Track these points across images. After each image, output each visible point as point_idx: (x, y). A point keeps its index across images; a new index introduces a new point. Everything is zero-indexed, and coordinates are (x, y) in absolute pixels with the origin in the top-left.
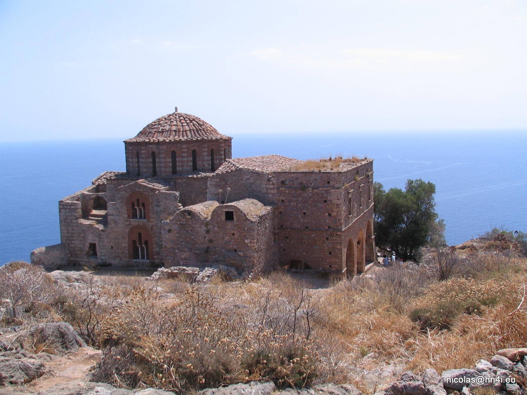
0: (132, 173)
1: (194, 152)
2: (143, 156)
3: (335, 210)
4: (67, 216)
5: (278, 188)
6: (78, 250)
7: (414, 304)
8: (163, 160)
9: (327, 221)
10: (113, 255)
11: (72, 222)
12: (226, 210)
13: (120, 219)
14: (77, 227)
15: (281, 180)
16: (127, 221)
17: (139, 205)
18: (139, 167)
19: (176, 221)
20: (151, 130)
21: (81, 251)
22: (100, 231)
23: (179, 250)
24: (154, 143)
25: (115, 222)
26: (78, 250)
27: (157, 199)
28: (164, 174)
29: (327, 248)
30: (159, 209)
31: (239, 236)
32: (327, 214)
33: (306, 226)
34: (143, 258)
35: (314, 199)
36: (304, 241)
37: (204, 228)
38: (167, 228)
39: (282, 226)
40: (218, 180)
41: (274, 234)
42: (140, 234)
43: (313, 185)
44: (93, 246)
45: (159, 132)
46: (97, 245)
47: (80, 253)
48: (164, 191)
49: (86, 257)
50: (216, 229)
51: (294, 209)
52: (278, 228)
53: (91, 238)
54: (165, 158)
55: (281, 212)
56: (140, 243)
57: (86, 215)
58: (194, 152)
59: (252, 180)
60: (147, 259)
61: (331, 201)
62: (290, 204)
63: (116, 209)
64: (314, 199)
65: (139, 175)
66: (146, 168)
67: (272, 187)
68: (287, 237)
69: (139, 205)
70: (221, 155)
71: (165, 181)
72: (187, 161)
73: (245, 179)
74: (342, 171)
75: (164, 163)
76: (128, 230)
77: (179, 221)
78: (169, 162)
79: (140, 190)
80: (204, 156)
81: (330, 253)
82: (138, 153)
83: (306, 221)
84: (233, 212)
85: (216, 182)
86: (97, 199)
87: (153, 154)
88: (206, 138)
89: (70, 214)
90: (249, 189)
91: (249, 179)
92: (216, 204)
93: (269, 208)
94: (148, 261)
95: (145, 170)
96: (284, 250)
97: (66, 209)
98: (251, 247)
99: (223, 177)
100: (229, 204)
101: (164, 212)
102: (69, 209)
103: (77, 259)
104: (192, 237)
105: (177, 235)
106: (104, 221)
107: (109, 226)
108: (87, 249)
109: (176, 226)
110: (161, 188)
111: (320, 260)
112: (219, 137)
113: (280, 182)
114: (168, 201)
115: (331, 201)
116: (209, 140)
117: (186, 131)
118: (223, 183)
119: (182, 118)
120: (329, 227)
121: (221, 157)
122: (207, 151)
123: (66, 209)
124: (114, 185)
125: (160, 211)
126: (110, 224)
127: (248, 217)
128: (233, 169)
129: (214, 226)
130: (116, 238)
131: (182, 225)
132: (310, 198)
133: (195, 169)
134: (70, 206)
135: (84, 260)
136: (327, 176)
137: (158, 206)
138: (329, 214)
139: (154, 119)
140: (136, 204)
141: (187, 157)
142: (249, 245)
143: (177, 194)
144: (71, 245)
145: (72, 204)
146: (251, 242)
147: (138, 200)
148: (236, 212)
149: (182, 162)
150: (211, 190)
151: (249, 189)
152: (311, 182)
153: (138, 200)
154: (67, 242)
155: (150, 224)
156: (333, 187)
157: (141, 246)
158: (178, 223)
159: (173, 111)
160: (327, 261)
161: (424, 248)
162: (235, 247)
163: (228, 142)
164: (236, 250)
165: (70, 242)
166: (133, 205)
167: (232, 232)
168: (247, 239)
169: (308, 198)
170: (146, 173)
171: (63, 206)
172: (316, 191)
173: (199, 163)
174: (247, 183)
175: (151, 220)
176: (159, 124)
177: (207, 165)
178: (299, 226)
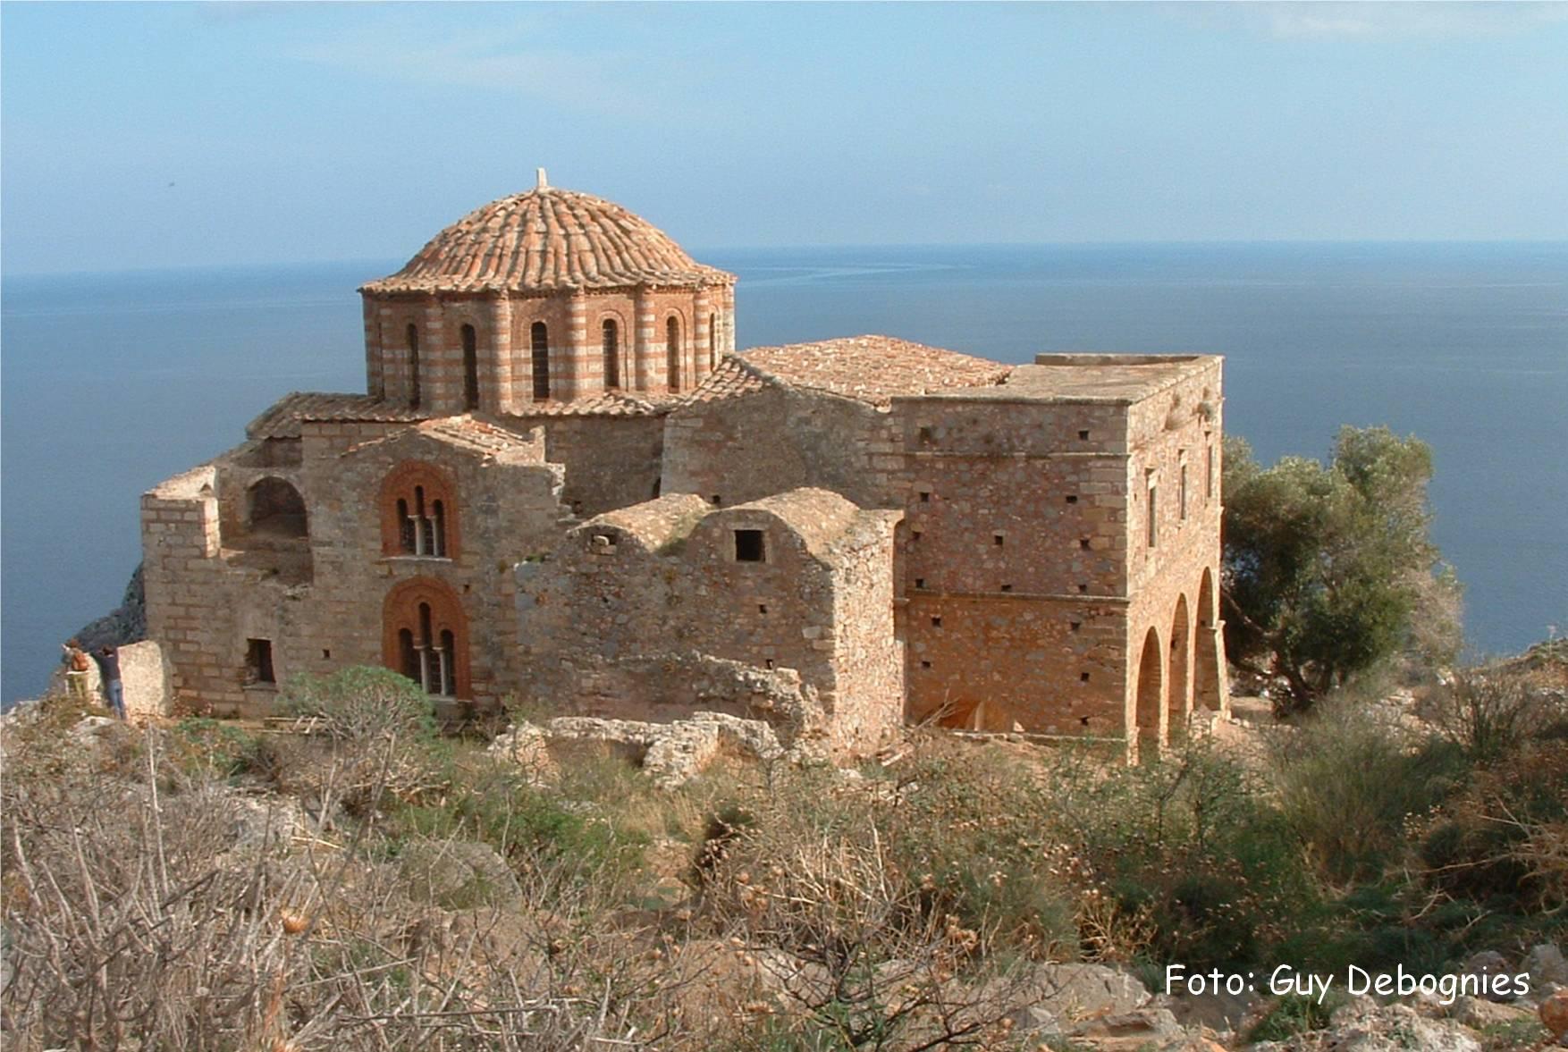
3: (1103, 528)
4: (169, 546)
6: (209, 665)
9: (1077, 567)
11: (186, 569)
12: (741, 527)
13: (354, 558)
15: (921, 424)
16: (380, 563)
19: (566, 563)
21: (219, 666)
23: (574, 661)
24: (468, 295)
25: (338, 566)
26: (209, 665)
27: (487, 490)
29: (1073, 659)
30: (491, 523)
31: (784, 616)
32: (1076, 544)
33: (1003, 582)
35: (1034, 491)
36: (994, 634)
37: (660, 589)
39: (920, 583)
43: (1029, 442)
46: (273, 644)
47: (215, 672)
49: (236, 687)
51: (964, 525)
55: (917, 535)
56: (427, 638)
59: (818, 425)
60: (451, 692)
61: (1090, 497)
62: (949, 507)
64: (1034, 491)
67: (887, 448)
68: (936, 622)
76: (384, 594)
77: (576, 563)
81: (1085, 677)
82: (412, 330)
83: (1002, 565)
84: (759, 532)
85: (696, 431)
87: (468, 330)
89: (180, 540)
90: (809, 454)
91: (807, 421)
92: (703, 506)
94: (451, 700)
96: (926, 664)
97: (167, 522)
100: (749, 506)
101: (510, 532)
102: (176, 522)
103: (204, 695)
104: (622, 618)
105: (568, 610)
107: (316, 581)
108: (240, 660)
109: (564, 581)
111: (1051, 698)
113: (917, 432)
114: (525, 495)
115: (1090, 497)
118: (719, 435)
123: (167, 522)
124: (331, 438)
125: (497, 531)
129: (697, 581)
130: (344, 623)
131: (587, 576)
132: (1020, 487)
134: (183, 511)
135: (228, 697)
136: (1079, 413)
137: (490, 511)
138: (1085, 544)
140: (412, 504)
142: (816, 645)
144: (182, 647)
147: (419, 490)
151: (809, 454)
152: (1023, 432)
153: (419, 490)
154: (171, 636)
155: (460, 573)
157: (429, 649)
158: (572, 569)
160: (1074, 703)
165: (180, 636)
166: (402, 505)
167: (760, 601)
168: (811, 624)
169: (1013, 486)
172: (1039, 463)
175: (465, 559)
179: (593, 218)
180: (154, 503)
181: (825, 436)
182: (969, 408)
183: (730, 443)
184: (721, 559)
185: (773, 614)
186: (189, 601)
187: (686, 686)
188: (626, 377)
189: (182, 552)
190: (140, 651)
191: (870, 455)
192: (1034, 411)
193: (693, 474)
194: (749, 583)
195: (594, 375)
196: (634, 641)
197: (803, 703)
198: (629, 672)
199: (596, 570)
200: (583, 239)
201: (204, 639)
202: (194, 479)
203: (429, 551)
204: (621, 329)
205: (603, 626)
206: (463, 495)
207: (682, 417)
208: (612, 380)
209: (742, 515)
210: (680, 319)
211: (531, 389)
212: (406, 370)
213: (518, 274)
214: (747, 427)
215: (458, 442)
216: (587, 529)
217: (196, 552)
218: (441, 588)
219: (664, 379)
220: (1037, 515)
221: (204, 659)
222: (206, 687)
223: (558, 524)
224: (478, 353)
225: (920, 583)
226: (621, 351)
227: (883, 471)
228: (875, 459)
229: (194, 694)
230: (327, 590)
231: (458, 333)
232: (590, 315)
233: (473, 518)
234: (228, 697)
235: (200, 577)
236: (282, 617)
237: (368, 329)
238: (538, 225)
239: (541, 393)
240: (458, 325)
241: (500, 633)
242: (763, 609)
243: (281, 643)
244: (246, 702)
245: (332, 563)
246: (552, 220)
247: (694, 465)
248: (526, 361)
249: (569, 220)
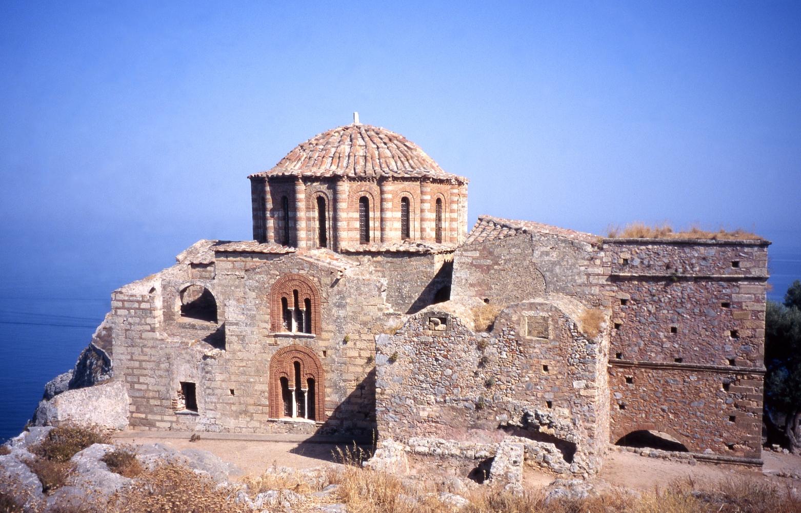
4: (130, 324)
6: (153, 398)
7: (33, 456)
10: (234, 408)
11: (141, 338)
13: (252, 332)
16: (268, 336)
21: (162, 399)
23: (415, 399)
25: (242, 338)
26: (153, 398)
33: (677, 356)
34: (301, 414)
40: (477, 254)
46: (197, 385)
47: (158, 402)
58: (405, 200)
61: (739, 304)
76: (271, 356)
77: (417, 335)
79: (302, 272)
89: (137, 320)
91: (547, 254)
97: (128, 309)
101: (354, 319)
102: (135, 309)
103: (150, 417)
115: (739, 304)
118: (489, 262)
123: (128, 309)
126: (231, 343)
130: (244, 373)
131: (425, 344)
134: (139, 302)
137: (340, 306)
138: (734, 334)
142: (582, 392)
144: (136, 386)
146: (587, 387)
151: (548, 274)
153: (296, 292)
154: (129, 379)
155: (322, 344)
158: (415, 339)
165: (136, 380)
166: (284, 301)
167: (544, 362)
168: (578, 379)
179: (390, 140)
180: (121, 297)
181: (559, 263)
183: (496, 267)
184: (518, 334)
185: (553, 370)
186: (142, 358)
187: (492, 417)
188: (414, 233)
189: (141, 328)
190: (108, 389)
191: (588, 275)
192: (702, 249)
193: (472, 285)
194: (537, 350)
195: (396, 229)
196: (456, 387)
197: (575, 432)
198: (453, 408)
199: (431, 340)
200: (387, 151)
201: (150, 382)
202: (146, 283)
203: (300, 329)
204: (412, 204)
205: (435, 377)
206: (324, 295)
207: (466, 250)
208: (406, 232)
210: (443, 200)
211: (358, 236)
213: (351, 166)
214: (508, 257)
215: (320, 263)
216: (426, 314)
217: (148, 328)
219: (433, 234)
221: (151, 394)
222: (152, 412)
223: (384, 314)
226: (411, 215)
227: (596, 285)
228: (591, 278)
229: (143, 416)
230: (234, 352)
232: (395, 194)
233: (330, 310)
234: (166, 418)
235: (150, 343)
236: (203, 369)
237: (254, 200)
238: (360, 142)
239: (365, 238)
241: (344, 381)
242: (546, 368)
243: (202, 385)
244: (177, 422)
245: (237, 336)
246: (367, 139)
247: (472, 280)
248: (356, 219)
249: (377, 140)
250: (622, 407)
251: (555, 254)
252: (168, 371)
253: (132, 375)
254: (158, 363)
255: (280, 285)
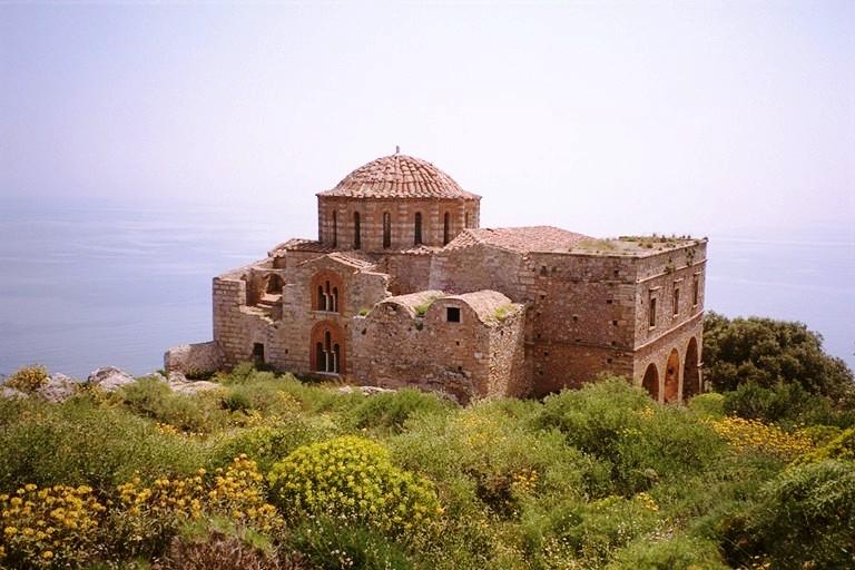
0: (327, 243)
1: (418, 214)
2: (341, 217)
5: (536, 278)
8: (372, 226)
12: (450, 306)
14: (238, 318)
17: (328, 291)
18: (335, 234)
20: (356, 180)
22: (269, 326)
24: (357, 199)
28: (371, 247)
30: (357, 298)
32: (611, 322)
38: (361, 328)
39: (539, 336)
40: (446, 259)
41: (526, 347)
42: (328, 334)
44: (259, 348)
45: (368, 182)
48: (367, 272)
50: (432, 333)
52: (534, 340)
53: (257, 336)
54: (373, 222)
56: (328, 348)
57: (253, 300)
58: (418, 214)
61: (618, 301)
63: (296, 295)
65: (334, 246)
66: (346, 235)
68: (546, 354)
69: (328, 291)
70: (461, 222)
71: (372, 256)
72: (407, 229)
73: (486, 260)
74: (640, 256)
75: (373, 233)
77: (379, 318)
78: (380, 229)
80: (432, 222)
82: (335, 213)
86: (266, 282)
87: (357, 214)
88: (437, 195)
91: (492, 261)
93: (519, 307)
95: (344, 239)
96: (541, 373)
98: (483, 365)
99: (454, 257)
101: (365, 303)
104: (397, 344)
106: (277, 310)
107: (284, 319)
110: (366, 267)
112: (458, 194)
115: (618, 301)
116: (442, 199)
117: (408, 183)
119: (404, 163)
120: (614, 343)
121: (459, 225)
122: (439, 215)
125: (359, 302)
127: (481, 318)
128: (471, 244)
133: (418, 241)
137: (356, 294)
138: (615, 323)
139: (364, 163)
140: (324, 289)
141: (407, 222)
142: (480, 361)
143: (386, 277)
145: (232, 284)
146: (483, 358)
147: (328, 282)
148: (464, 312)
149: (399, 229)
150: (436, 274)
156: (624, 281)
159: (392, 152)
161: (327, 416)
162: (460, 363)
163: (474, 202)
164: (460, 368)
166: (320, 288)
167: (457, 340)
168: (478, 352)
170: (344, 243)
171: (219, 286)
172: (595, 285)
173: (425, 234)
174: (486, 267)
176: (369, 171)
177: (438, 235)
178: (566, 338)
179: (418, 169)
182: (564, 258)
184: (440, 320)
185: (462, 346)
203: (331, 309)
209: (450, 300)
212: (332, 230)
218: (336, 326)
220: (593, 308)
224: (361, 225)
225: (539, 336)
231: (352, 215)
240: (353, 211)
249: (405, 168)
250: (541, 373)
251: (497, 261)
252: (651, 291)
253: (224, 336)
254: (241, 329)
255: (318, 277)
